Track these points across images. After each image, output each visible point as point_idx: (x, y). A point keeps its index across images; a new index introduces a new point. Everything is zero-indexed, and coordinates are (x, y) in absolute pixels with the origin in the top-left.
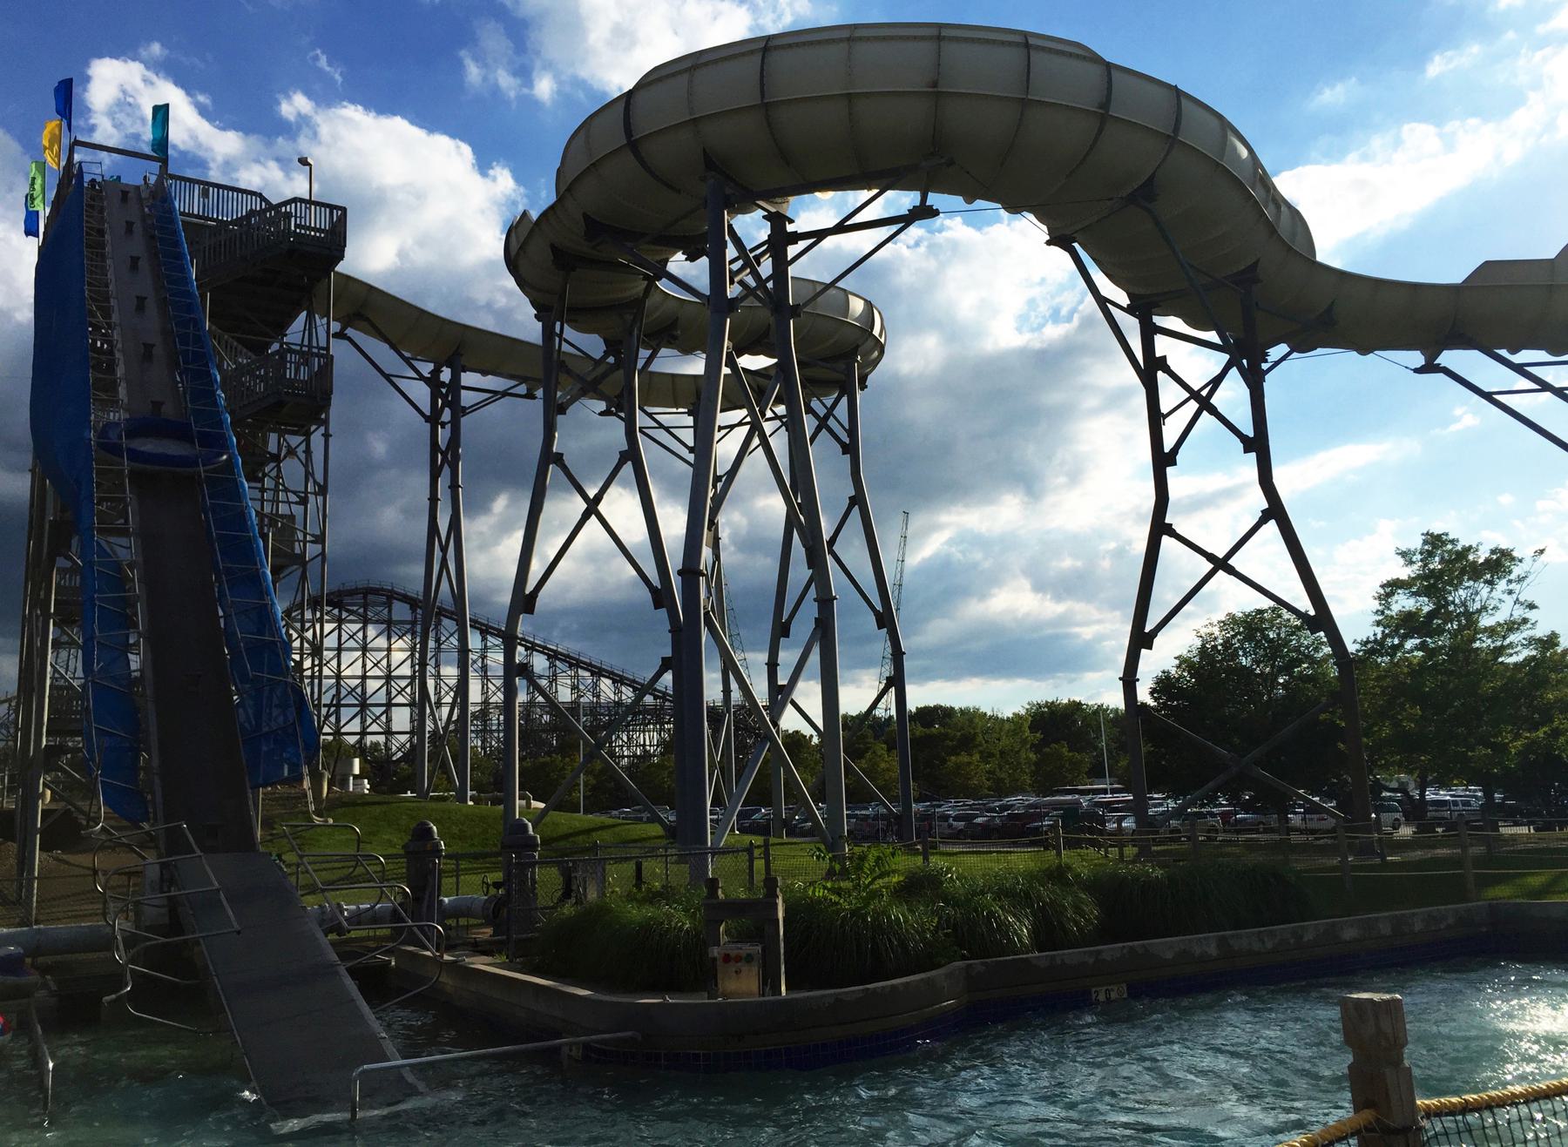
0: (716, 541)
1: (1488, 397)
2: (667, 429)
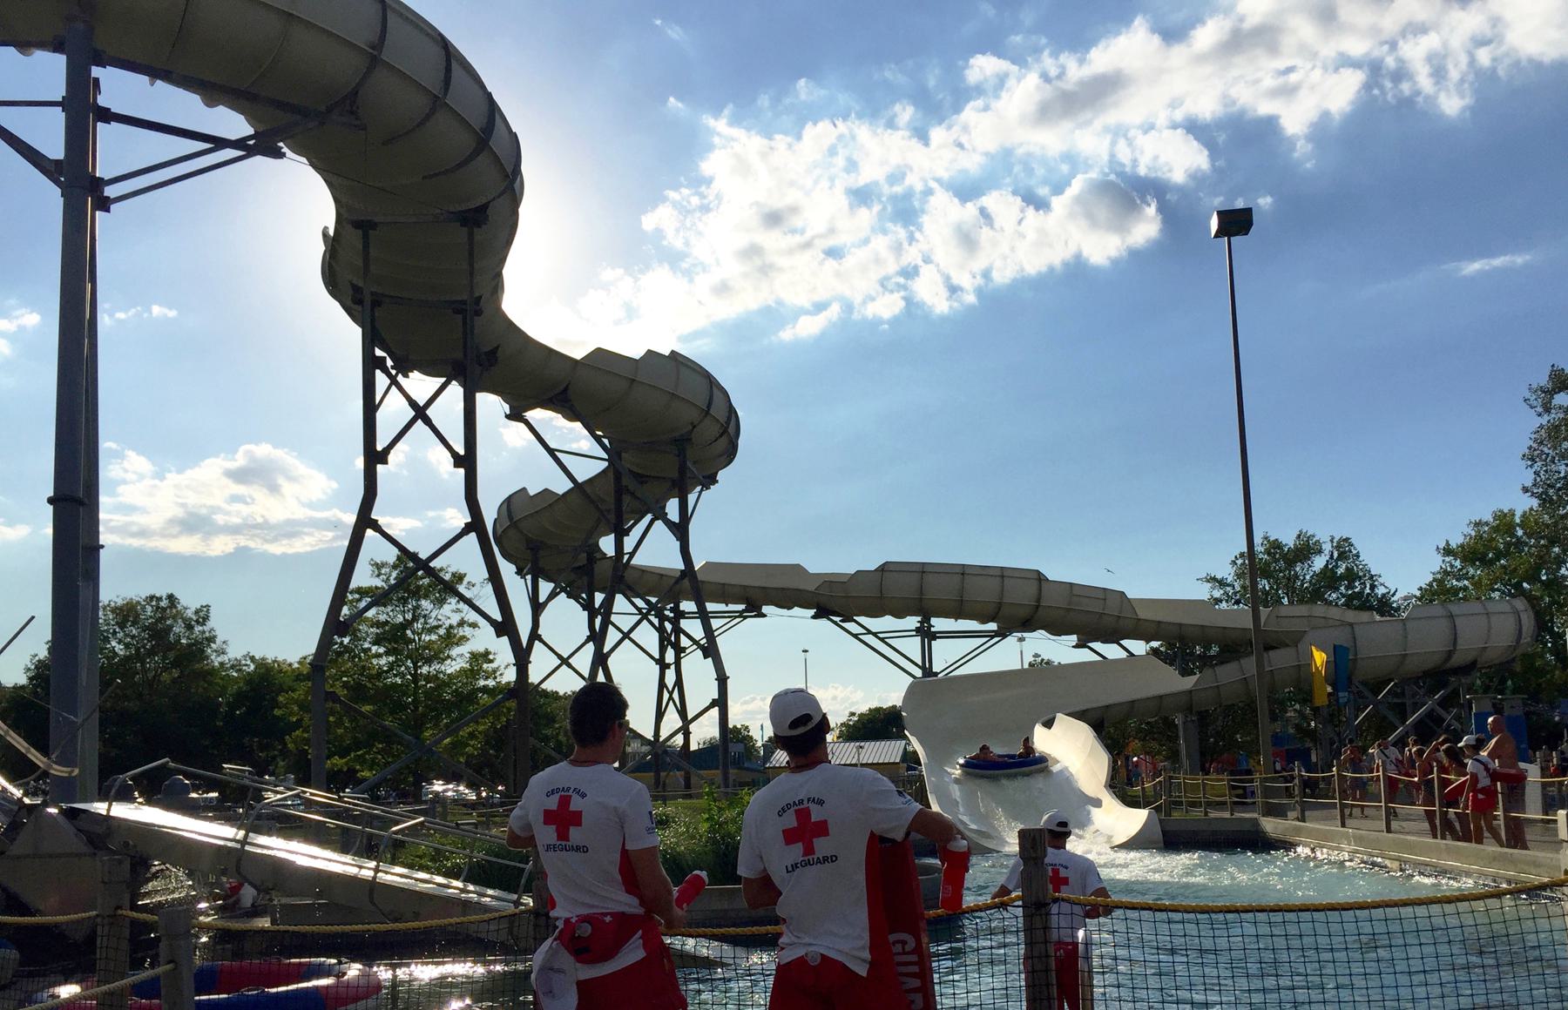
2: (875, 634)
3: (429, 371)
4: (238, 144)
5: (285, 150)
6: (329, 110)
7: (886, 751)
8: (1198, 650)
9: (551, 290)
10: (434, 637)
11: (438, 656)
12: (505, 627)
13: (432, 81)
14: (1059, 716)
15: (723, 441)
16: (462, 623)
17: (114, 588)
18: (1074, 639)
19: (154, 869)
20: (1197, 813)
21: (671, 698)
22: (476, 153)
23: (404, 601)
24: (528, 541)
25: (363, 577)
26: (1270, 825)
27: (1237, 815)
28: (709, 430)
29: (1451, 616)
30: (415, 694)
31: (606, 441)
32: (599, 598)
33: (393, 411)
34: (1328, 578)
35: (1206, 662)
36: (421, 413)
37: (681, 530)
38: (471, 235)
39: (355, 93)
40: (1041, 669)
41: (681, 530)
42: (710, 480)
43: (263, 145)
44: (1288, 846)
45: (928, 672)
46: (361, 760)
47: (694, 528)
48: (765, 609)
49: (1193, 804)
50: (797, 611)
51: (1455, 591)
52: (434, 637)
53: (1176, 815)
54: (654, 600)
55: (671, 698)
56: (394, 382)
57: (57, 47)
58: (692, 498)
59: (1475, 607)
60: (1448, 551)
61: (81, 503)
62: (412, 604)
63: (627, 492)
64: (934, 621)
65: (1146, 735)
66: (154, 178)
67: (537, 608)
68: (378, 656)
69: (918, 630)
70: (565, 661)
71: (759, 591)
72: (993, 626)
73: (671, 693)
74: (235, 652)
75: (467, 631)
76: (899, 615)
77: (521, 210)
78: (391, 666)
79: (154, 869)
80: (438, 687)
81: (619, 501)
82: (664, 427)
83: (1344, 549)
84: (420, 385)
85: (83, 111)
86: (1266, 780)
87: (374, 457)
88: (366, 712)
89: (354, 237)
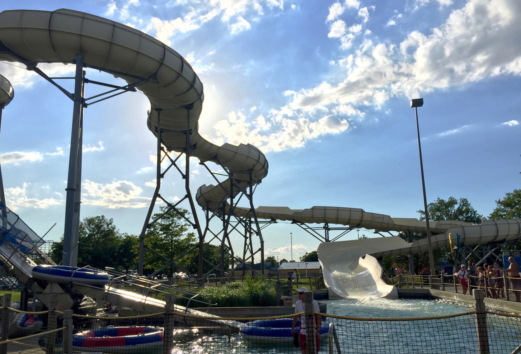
0: (337, 343)
1: (212, 174)
2: (311, 229)
3: (177, 150)
4: (124, 88)
5: (137, 89)
6: (149, 78)
7: (312, 265)
8: (415, 234)
9: (216, 124)
10: (177, 229)
11: (178, 234)
12: (197, 226)
13: (178, 69)
14: (367, 255)
15: (263, 170)
16: (185, 225)
17: (84, 216)
18: (374, 230)
19: (84, 298)
20: (411, 287)
21: (248, 248)
22: (190, 88)
23: (169, 218)
24: (206, 200)
25: (156, 210)
26: (433, 292)
27: (424, 288)
28: (258, 167)
29: (496, 224)
30: (171, 246)
31: (228, 171)
32: (226, 217)
33: (165, 164)
34: (460, 212)
35: (418, 238)
36: (173, 163)
37: (250, 197)
38: (188, 111)
39: (156, 73)
40: (364, 240)
41: (250, 197)
42: (259, 182)
43: (130, 88)
44: (438, 298)
45: (327, 240)
46: (155, 266)
47: (254, 196)
48: (277, 221)
49: (411, 284)
50: (287, 221)
51: (502, 216)
52: (177, 229)
53: (404, 288)
54: (242, 218)
55: (248, 248)
56: (166, 154)
57: (74, 62)
58: (253, 187)
59: (505, 221)
60: (499, 202)
61: (74, 190)
62: (171, 219)
63: (232, 187)
64: (329, 224)
65: (398, 261)
66: (99, 98)
67: (208, 220)
68: (161, 234)
69: (324, 227)
70: (216, 236)
71: (274, 215)
72: (348, 226)
73: (248, 246)
74: (121, 232)
75: (187, 227)
76: (318, 222)
77: (203, 104)
78: (165, 237)
79: (84, 298)
80: (178, 244)
81: (232, 189)
82: (246, 167)
83: (465, 202)
84: (173, 154)
85: (80, 79)
86: (432, 277)
87: (160, 176)
88: (156, 253)
89: (156, 113)
